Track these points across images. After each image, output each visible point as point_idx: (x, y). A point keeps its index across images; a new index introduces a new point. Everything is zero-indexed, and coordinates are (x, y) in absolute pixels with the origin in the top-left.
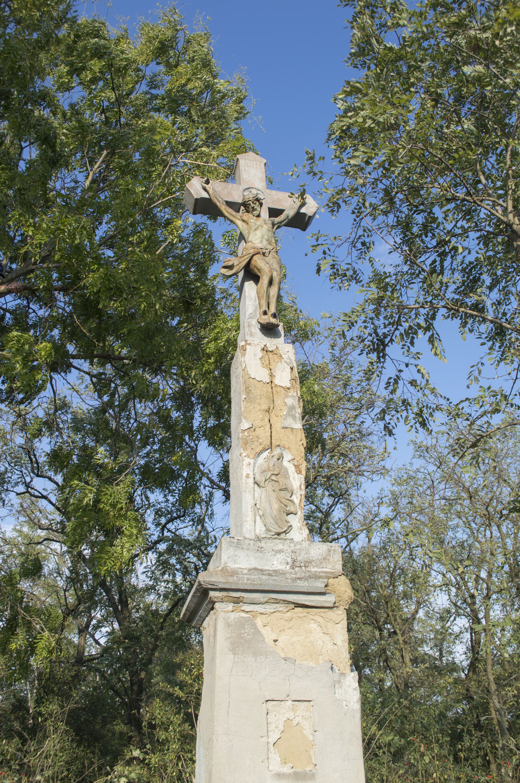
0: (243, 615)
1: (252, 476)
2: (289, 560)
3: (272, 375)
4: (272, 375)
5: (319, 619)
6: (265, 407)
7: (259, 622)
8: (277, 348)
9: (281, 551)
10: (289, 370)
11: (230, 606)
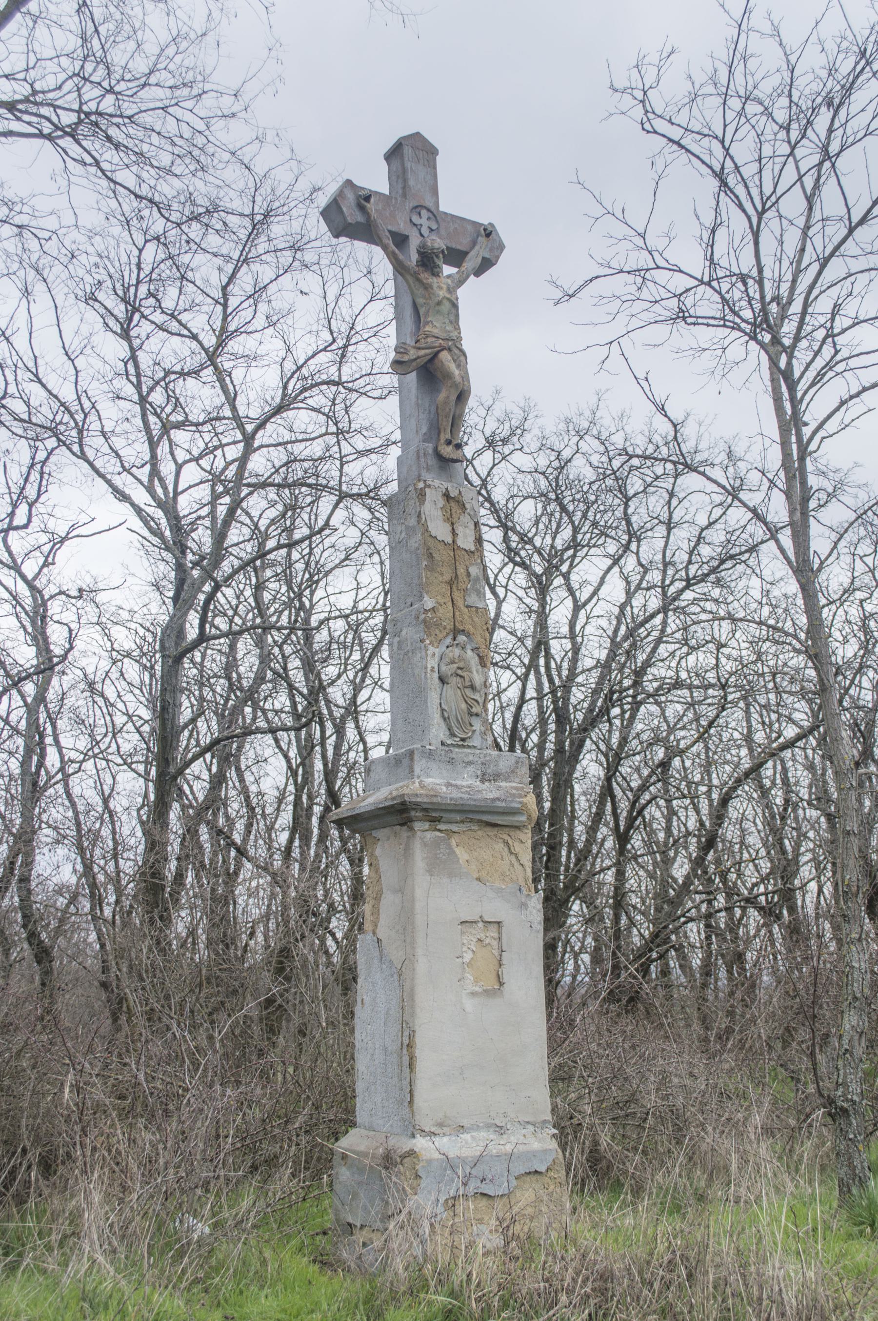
0: (438, 834)
1: (436, 669)
2: (479, 772)
3: (454, 533)
4: (454, 533)
5: (506, 837)
6: (447, 577)
7: (453, 842)
8: (460, 493)
9: (471, 763)
10: (473, 527)
11: (427, 825)
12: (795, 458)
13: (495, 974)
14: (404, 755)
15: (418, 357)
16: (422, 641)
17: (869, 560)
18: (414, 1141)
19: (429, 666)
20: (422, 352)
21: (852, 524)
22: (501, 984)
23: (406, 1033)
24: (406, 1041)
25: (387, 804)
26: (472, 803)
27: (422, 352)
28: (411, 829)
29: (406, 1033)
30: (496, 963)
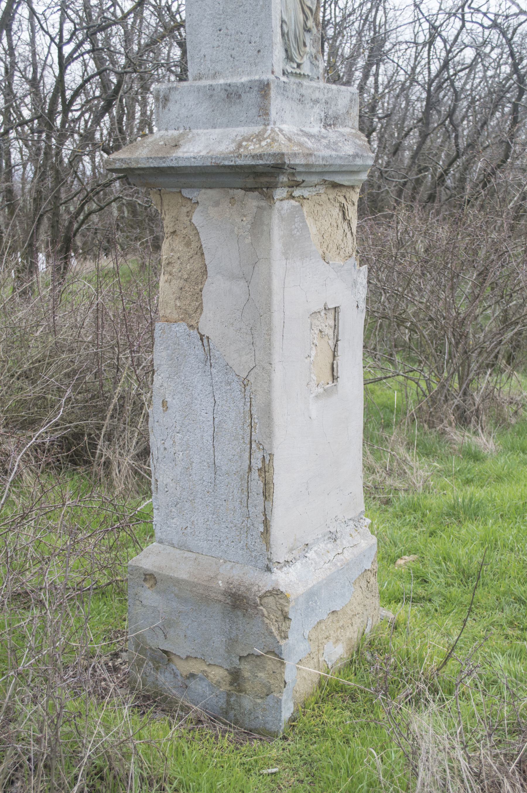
13: (329, 366)
14: (250, 87)
18: (274, 577)
22: (334, 378)
23: (258, 455)
24: (257, 464)
25: (226, 163)
26: (339, 162)
28: (270, 198)
29: (258, 455)
30: (331, 354)
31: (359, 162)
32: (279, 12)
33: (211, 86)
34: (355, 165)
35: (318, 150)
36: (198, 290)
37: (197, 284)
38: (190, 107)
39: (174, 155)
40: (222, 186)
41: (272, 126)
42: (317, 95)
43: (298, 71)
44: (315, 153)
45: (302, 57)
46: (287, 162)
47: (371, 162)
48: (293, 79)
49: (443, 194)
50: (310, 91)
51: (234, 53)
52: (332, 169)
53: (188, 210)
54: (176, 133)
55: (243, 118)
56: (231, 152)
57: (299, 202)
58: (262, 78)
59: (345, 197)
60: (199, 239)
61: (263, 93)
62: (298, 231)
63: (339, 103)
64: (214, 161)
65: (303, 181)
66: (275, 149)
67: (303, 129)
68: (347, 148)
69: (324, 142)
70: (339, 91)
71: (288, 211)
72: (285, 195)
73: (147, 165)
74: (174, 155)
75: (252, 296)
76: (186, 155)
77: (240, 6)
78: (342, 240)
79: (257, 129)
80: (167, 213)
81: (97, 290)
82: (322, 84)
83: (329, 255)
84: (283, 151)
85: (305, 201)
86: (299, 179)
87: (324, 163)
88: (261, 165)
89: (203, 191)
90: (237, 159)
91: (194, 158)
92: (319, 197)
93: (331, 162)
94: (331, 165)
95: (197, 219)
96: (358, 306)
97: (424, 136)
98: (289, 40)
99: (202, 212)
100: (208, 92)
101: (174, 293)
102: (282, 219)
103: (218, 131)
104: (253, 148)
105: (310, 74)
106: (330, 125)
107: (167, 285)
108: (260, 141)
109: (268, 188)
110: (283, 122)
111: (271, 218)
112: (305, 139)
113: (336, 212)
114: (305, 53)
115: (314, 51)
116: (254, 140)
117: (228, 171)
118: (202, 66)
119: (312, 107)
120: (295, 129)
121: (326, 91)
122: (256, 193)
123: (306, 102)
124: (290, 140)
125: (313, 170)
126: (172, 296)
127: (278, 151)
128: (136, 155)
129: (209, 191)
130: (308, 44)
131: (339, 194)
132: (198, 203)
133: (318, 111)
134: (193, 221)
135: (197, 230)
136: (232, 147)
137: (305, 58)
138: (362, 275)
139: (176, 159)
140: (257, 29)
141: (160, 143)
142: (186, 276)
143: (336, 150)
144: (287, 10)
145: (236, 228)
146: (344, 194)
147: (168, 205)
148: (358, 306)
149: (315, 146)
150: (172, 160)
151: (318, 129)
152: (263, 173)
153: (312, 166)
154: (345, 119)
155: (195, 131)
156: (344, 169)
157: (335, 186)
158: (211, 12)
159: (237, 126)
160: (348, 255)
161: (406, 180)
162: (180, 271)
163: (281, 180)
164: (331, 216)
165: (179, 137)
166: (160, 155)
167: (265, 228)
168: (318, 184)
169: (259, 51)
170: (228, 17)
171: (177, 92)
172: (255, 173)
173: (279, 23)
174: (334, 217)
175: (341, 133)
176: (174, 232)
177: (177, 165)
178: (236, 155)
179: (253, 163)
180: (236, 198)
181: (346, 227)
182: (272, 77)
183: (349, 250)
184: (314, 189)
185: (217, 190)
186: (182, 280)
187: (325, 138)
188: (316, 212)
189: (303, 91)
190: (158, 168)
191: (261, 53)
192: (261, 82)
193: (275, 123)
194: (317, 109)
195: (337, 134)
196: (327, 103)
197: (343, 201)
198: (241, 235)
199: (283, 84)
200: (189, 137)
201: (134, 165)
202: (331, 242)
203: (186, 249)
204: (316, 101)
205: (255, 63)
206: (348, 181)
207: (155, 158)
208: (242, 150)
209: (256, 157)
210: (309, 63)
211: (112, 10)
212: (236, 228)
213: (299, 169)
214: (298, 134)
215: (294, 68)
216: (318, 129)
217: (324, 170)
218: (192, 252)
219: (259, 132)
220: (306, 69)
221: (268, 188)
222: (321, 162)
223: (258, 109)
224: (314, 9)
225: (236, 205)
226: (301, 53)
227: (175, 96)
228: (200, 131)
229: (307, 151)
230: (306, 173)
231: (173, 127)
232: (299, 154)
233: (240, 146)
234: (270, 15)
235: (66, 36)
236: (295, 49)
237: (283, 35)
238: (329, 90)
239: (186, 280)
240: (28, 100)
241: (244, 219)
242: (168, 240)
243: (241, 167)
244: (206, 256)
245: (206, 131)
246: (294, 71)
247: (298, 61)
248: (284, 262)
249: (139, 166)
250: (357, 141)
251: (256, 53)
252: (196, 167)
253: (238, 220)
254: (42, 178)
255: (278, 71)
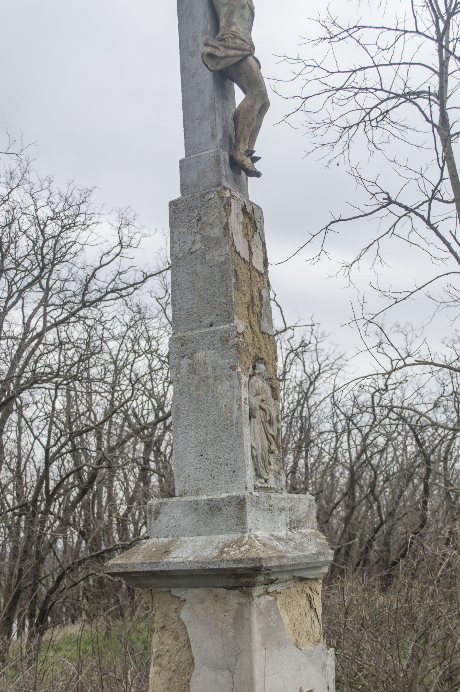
12: (228, 325)
14: (229, 501)
15: (228, 57)
16: (233, 368)
17: (3, 578)
19: (243, 397)
20: (232, 52)
21: (432, 363)
25: (211, 567)
26: (305, 560)
27: (232, 52)
28: (249, 595)
31: (321, 559)
32: (249, 441)
33: (196, 501)
34: (319, 562)
35: (288, 552)
36: (185, 681)
37: (184, 675)
38: (178, 518)
39: (165, 560)
40: (207, 586)
41: (249, 533)
42: (283, 504)
43: (266, 485)
44: (286, 555)
45: (268, 474)
46: (264, 565)
47: (331, 558)
48: (263, 494)
49: (373, 556)
50: (277, 502)
51: (213, 473)
52: (300, 567)
53: (177, 607)
54: (166, 540)
55: (223, 527)
56: (215, 558)
57: (273, 596)
58: (238, 495)
59: (310, 588)
60: (187, 633)
61: (240, 506)
62: (274, 623)
63: (300, 509)
64: (200, 565)
65: (277, 579)
66: (253, 554)
67: (274, 533)
68: (311, 547)
69: (292, 543)
70: (299, 499)
71: (265, 605)
72: (262, 591)
73: (142, 569)
74: (165, 560)
75: (236, 686)
76: (176, 560)
77: (218, 437)
78: (311, 627)
79: (236, 536)
80: (157, 610)
81: (77, 668)
82: (285, 494)
83: (301, 642)
84: (261, 556)
85: (278, 595)
86: (273, 577)
87: (294, 563)
88: (242, 568)
89: (190, 590)
90: (221, 563)
91: (183, 563)
92: (289, 590)
93: (299, 561)
94: (299, 564)
95: (184, 615)
96: (328, 688)
97: (351, 508)
98: (257, 461)
99: (189, 609)
100: (193, 506)
101: (163, 684)
102: (260, 613)
103: (202, 538)
104: (233, 553)
105: (275, 487)
106: (294, 528)
107: (157, 676)
108: (240, 547)
109: (247, 587)
110: (257, 529)
111: (250, 613)
112: (276, 543)
113: (304, 602)
114: (270, 470)
115: (277, 468)
116: (234, 546)
117: (213, 573)
118: (187, 484)
119: (280, 515)
120: (267, 535)
121: (289, 500)
122: (237, 591)
123: (274, 511)
124: (264, 545)
125: (285, 569)
126: (161, 687)
127: (256, 556)
128: (132, 560)
129: (196, 591)
130: (272, 463)
131: (306, 586)
132: (185, 600)
133: (284, 517)
134: (181, 617)
135: (184, 625)
136: (216, 552)
137: (271, 474)
138: (329, 658)
139: (167, 564)
140: (232, 454)
141: (153, 550)
142: (174, 668)
143: (302, 551)
144: (255, 438)
145: (220, 623)
146: (309, 586)
147: (159, 603)
148: (328, 688)
149: (285, 548)
150: (163, 565)
151: (285, 532)
152: (243, 574)
153: (284, 566)
154: (306, 521)
155: (182, 539)
156: (310, 566)
157: (302, 579)
158: (193, 442)
159: (219, 534)
160: (316, 640)
161: (339, 546)
162: (169, 663)
163: (259, 580)
164: (300, 606)
165: (169, 544)
166: (153, 561)
167: (246, 622)
168: (289, 580)
169: (234, 472)
170: (208, 445)
171: (167, 507)
172: (236, 574)
173: (249, 449)
174: (302, 606)
175: (303, 534)
176: (164, 627)
177: (168, 569)
178: (219, 559)
179: (235, 566)
180: (219, 596)
181: (313, 615)
182: (246, 493)
183: (317, 635)
184: (285, 584)
185: (203, 589)
186: (171, 672)
187: (291, 540)
188: (287, 604)
189: (272, 503)
190: (151, 572)
191: (236, 473)
192: (238, 497)
193: (251, 531)
194: (283, 516)
195: (301, 535)
196: (290, 510)
197: (310, 592)
198: (225, 629)
199: (255, 498)
200: (177, 544)
201: (130, 569)
202: (302, 629)
203: (174, 643)
204: (282, 510)
205: (231, 481)
206: (313, 575)
207: (148, 564)
208: (225, 555)
209: (237, 561)
210: (273, 478)
211: (87, 414)
212: (220, 623)
213: (273, 570)
214: (270, 539)
215: (262, 483)
216: (285, 532)
217: (294, 568)
218: (180, 645)
219: (238, 539)
220: (272, 483)
221: (247, 587)
222: (291, 563)
223: (236, 519)
224: (275, 435)
225: (219, 602)
226: (268, 471)
227: (165, 510)
228: (186, 539)
229: (279, 554)
230: (279, 572)
231: (163, 535)
232: (273, 557)
233: (222, 551)
234: (243, 444)
235: (52, 442)
236: (262, 468)
237: (253, 458)
238: (292, 499)
239: (174, 672)
240: (11, 487)
241: (227, 614)
242: (158, 634)
243: (224, 570)
244: (193, 649)
245: (191, 538)
246: (263, 485)
247: (265, 477)
248: (263, 652)
249: (135, 570)
250: (318, 540)
251: (231, 473)
252: (185, 570)
253: (221, 615)
254: (24, 557)
255: (250, 486)
